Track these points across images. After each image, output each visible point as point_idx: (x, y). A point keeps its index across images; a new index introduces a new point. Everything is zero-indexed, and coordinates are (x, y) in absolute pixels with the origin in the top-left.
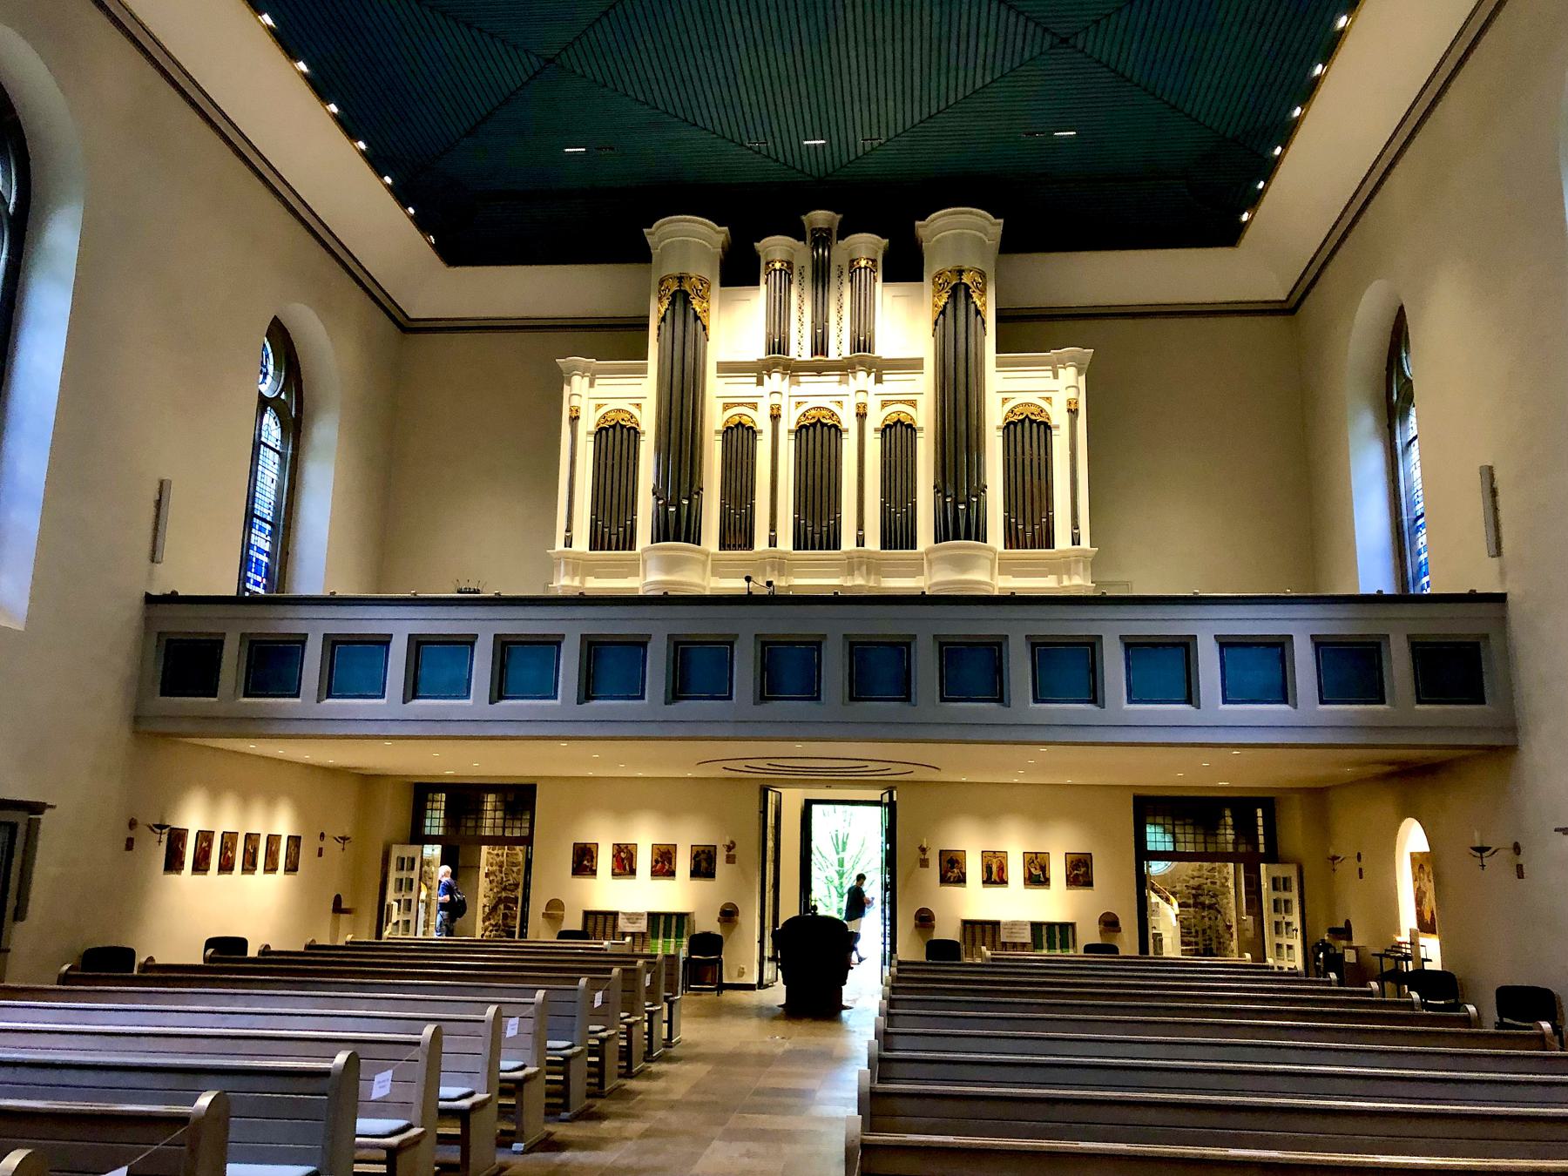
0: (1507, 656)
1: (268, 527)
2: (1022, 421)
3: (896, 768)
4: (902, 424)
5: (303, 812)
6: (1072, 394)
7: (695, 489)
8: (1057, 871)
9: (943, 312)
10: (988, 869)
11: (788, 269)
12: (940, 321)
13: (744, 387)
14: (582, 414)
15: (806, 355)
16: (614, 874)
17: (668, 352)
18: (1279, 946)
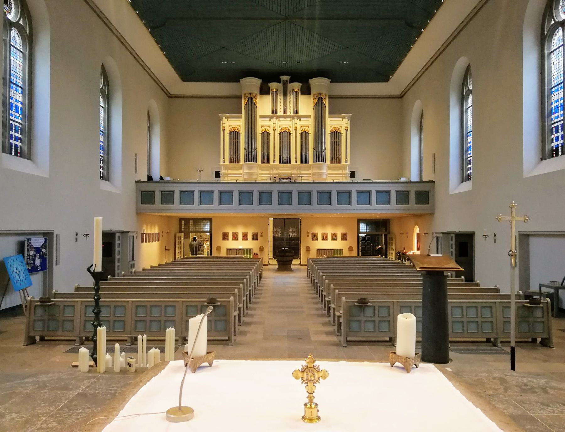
0: (434, 195)
5: (159, 229)
6: (346, 125)
8: (339, 237)
9: (316, 104)
10: (323, 237)
13: (266, 122)
15: (282, 114)
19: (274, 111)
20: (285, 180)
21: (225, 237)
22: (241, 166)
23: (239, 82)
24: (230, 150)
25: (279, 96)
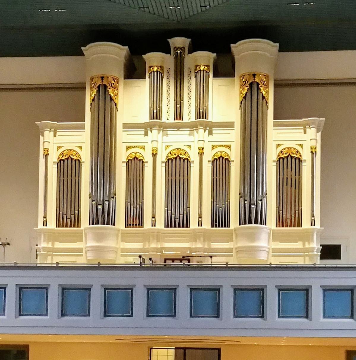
2: (287, 157)
6: (313, 143)
9: (245, 97)
13: (137, 137)
14: (50, 152)
15: (171, 120)
17: (96, 119)
19: (156, 115)
20: (177, 263)
22: (81, 232)
23: (82, 54)
24: (58, 200)
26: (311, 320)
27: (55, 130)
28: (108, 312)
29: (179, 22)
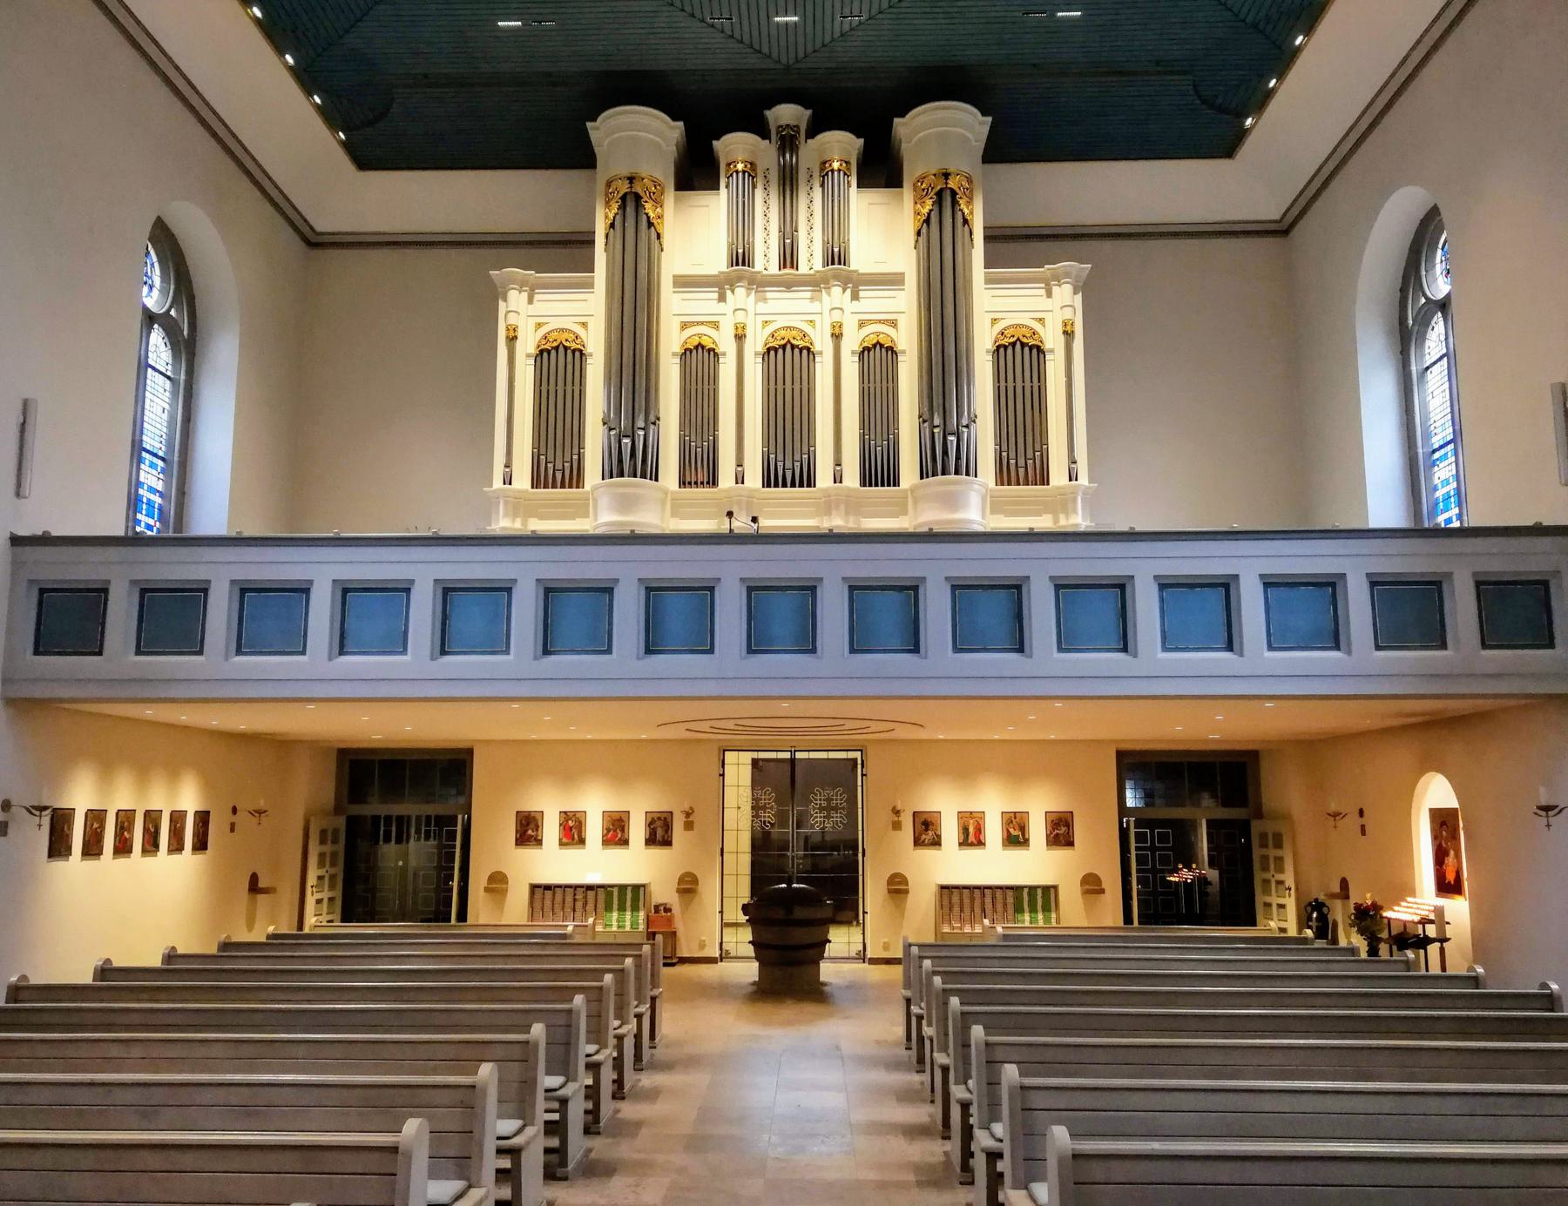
1: (160, 463)
2: (1014, 344)
3: (874, 726)
4: (882, 346)
5: (209, 786)
6: (1068, 314)
7: (652, 418)
8: (1037, 830)
9: (927, 221)
10: (965, 830)
11: (751, 171)
12: (924, 230)
13: (703, 303)
14: (520, 334)
15: (774, 268)
16: (561, 844)
18: (1268, 905)
19: (741, 258)
21: (528, 830)
25: (759, 193)
26: (1135, 656)
27: (532, 290)
28: (655, 644)
29: (788, 68)
